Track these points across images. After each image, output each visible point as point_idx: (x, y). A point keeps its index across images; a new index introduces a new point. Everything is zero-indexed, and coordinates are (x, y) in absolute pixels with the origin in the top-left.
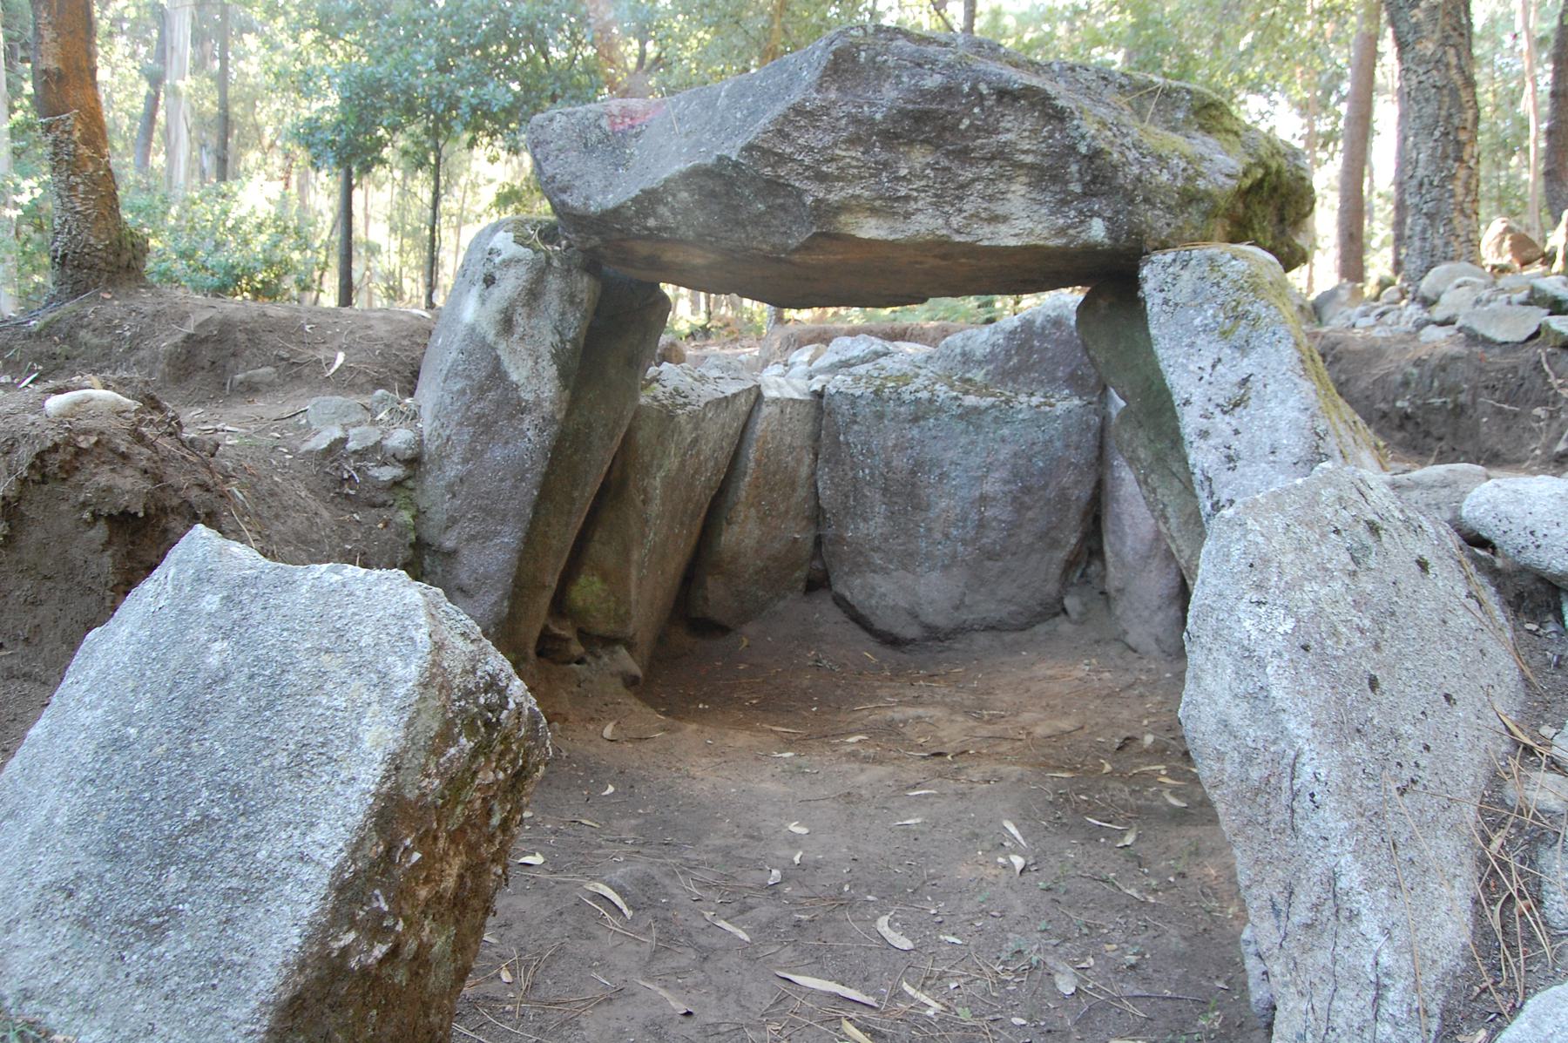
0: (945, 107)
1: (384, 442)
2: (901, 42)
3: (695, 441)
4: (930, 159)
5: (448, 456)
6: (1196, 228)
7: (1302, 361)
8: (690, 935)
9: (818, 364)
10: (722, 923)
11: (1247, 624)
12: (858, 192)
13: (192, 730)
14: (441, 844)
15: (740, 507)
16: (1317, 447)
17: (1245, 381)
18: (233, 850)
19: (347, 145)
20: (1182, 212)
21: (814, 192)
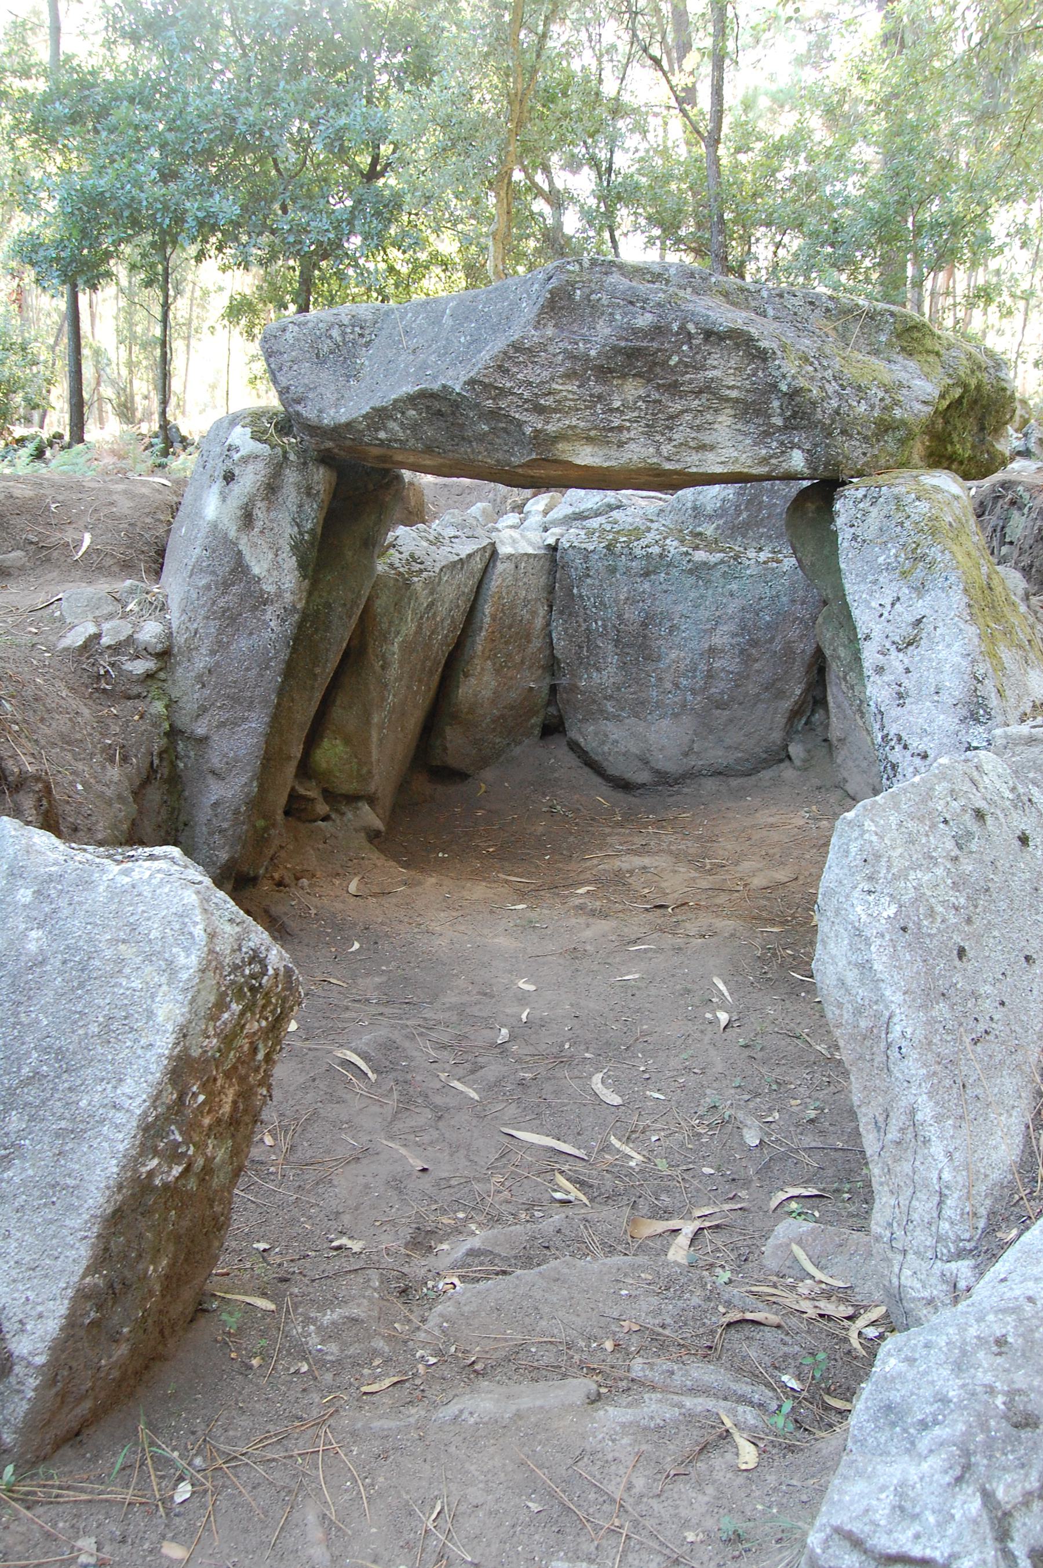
0: (655, 345)
1: (136, 636)
2: (615, 278)
3: (431, 605)
4: (642, 392)
5: (196, 649)
6: (892, 455)
7: (969, 606)
8: (427, 1096)
9: (553, 515)
10: (456, 1084)
11: (859, 909)
12: (574, 423)
13: (20, 1003)
14: (219, 1083)
15: (476, 661)
16: (976, 690)
17: (919, 621)
18: (60, 1099)
19: (72, 261)
20: (878, 441)
21: (533, 423)
